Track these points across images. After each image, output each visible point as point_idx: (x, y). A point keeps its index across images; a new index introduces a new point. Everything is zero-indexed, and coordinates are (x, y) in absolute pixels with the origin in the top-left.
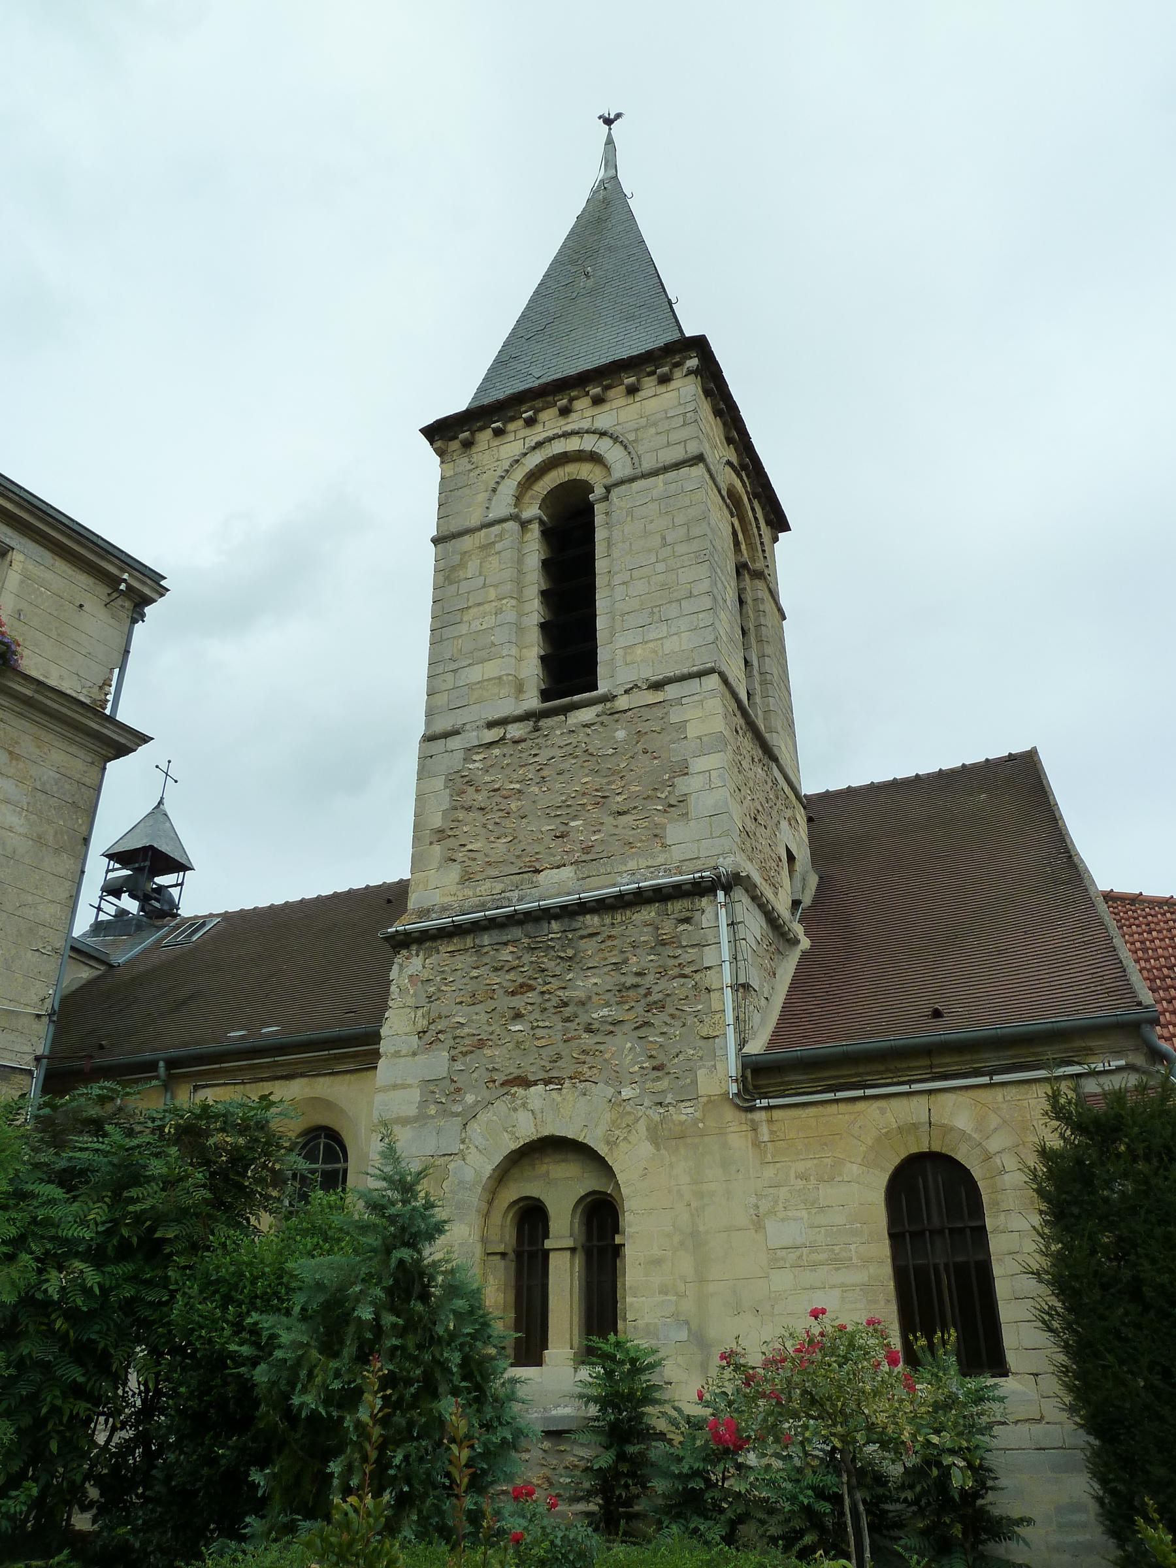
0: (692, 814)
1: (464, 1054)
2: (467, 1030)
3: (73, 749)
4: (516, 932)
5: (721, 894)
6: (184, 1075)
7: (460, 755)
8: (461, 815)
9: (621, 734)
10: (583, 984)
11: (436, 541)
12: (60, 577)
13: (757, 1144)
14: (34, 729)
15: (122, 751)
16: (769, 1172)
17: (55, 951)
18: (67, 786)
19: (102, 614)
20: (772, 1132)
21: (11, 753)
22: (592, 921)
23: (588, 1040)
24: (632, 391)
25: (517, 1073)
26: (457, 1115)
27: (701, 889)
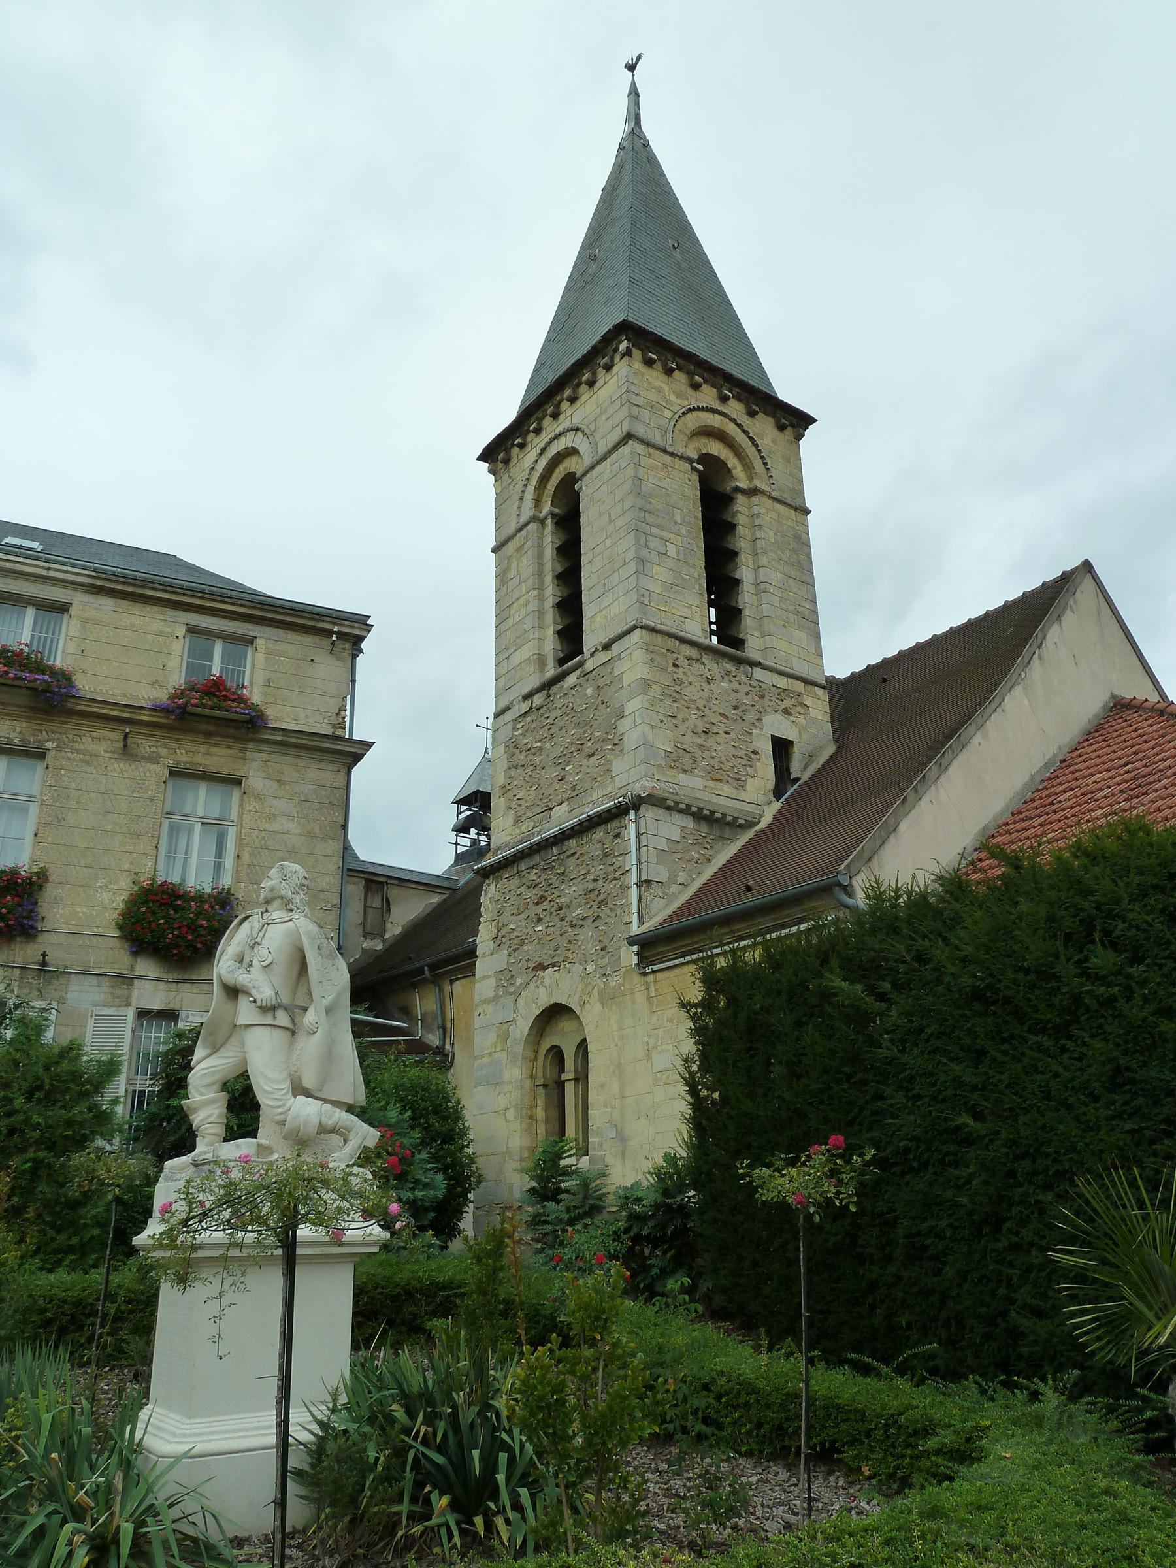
0: (626, 750)
1: (515, 950)
2: (516, 934)
3: (323, 765)
4: (536, 859)
5: (632, 813)
6: (443, 974)
7: (510, 726)
8: (513, 772)
9: (589, 691)
10: (571, 890)
11: (495, 550)
12: (294, 644)
13: (649, 998)
14: (291, 760)
15: (357, 758)
16: (654, 1019)
17: (334, 906)
18: (323, 793)
19: (330, 660)
20: (656, 990)
21: (278, 781)
22: (572, 843)
23: (572, 932)
24: (591, 384)
25: (539, 960)
26: (512, 994)
27: (618, 812)
